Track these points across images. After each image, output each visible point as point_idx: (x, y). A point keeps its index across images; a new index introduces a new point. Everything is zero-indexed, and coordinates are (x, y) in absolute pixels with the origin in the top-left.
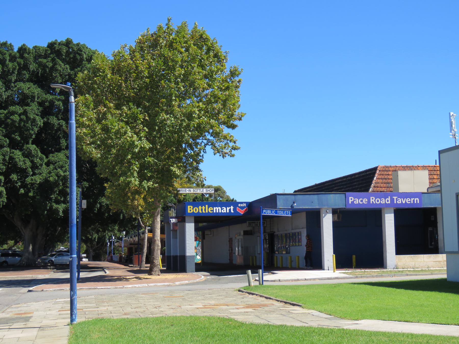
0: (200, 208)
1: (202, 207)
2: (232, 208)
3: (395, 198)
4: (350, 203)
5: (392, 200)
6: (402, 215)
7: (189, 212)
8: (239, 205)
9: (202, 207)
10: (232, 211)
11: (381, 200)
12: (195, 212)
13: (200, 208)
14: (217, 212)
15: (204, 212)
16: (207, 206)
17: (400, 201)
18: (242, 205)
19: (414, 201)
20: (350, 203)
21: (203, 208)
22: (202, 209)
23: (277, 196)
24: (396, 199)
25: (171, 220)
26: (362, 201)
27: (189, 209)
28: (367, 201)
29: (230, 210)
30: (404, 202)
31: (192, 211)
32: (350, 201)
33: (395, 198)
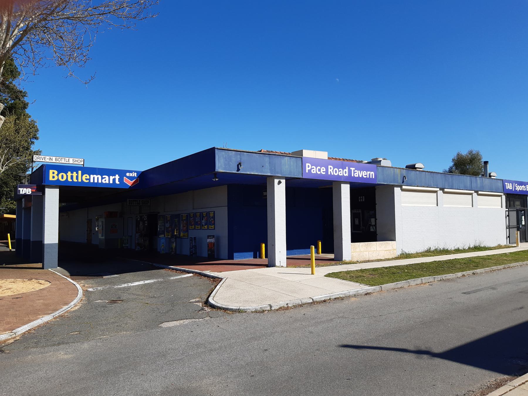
0: (69, 174)
1: (72, 173)
2: (117, 177)
3: (353, 169)
4: (307, 171)
5: (350, 171)
6: (297, 189)
7: (51, 179)
8: (128, 174)
9: (72, 173)
10: (117, 182)
11: (339, 171)
12: (60, 179)
13: (69, 174)
14: (96, 181)
15: (75, 180)
16: (80, 172)
17: (357, 173)
18: (131, 175)
19: (370, 174)
20: (307, 171)
21: (75, 174)
22: (72, 177)
23: (216, 151)
24: (354, 170)
25: (21, 189)
26: (319, 170)
27: (51, 175)
28: (325, 170)
29: (114, 180)
30: (360, 176)
31: (56, 178)
32: (307, 169)
33: (353, 169)
